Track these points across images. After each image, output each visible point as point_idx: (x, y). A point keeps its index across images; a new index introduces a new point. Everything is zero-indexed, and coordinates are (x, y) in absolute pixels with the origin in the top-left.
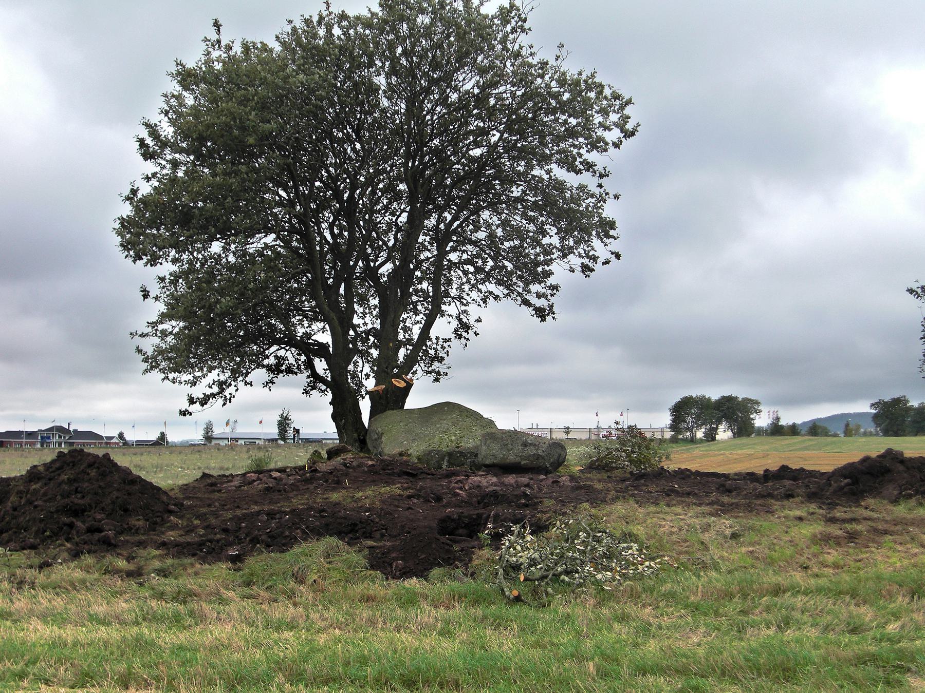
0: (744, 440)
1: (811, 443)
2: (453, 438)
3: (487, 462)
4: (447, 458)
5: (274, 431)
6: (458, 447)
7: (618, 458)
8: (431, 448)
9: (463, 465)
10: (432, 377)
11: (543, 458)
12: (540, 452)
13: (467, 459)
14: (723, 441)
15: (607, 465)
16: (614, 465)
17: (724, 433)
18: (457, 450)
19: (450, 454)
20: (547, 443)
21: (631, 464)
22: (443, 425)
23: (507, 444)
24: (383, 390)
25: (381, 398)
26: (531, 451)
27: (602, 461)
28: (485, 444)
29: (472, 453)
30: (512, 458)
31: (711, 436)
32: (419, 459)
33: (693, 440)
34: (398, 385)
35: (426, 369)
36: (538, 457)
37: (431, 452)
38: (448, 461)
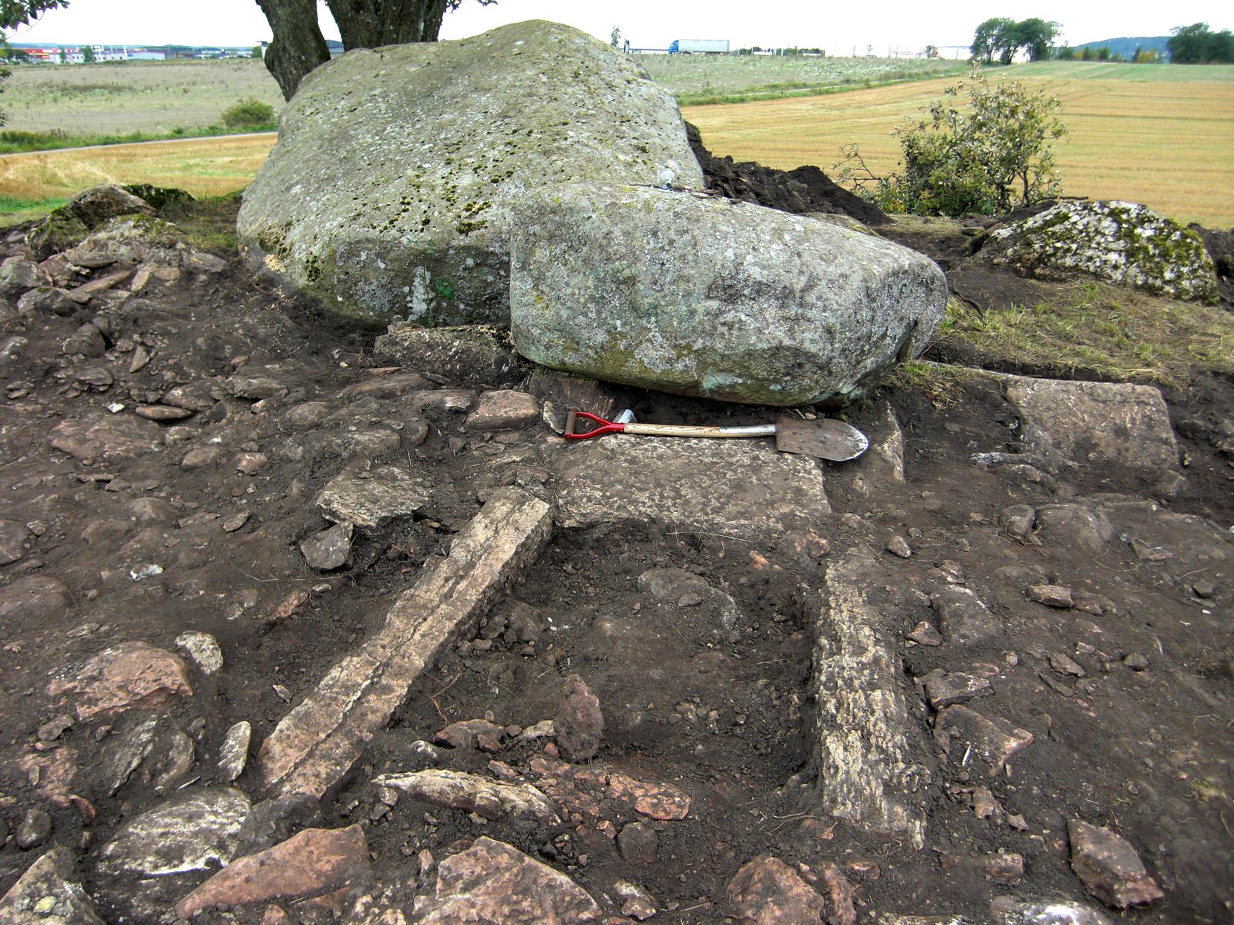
0: (1040, 65)
1: (1108, 70)
5: (609, 41)
6: (466, 229)
7: (1089, 235)
8: (359, 230)
11: (825, 367)
12: (810, 340)
14: (1022, 65)
15: (1042, 260)
16: (1069, 261)
17: (1021, 55)
18: (461, 240)
20: (856, 281)
21: (1129, 263)
23: (631, 281)
27: (1029, 244)
31: (1006, 60)
32: (314, 273)
33: (989, 63)
37: (353, 248)
38: (432, 286)
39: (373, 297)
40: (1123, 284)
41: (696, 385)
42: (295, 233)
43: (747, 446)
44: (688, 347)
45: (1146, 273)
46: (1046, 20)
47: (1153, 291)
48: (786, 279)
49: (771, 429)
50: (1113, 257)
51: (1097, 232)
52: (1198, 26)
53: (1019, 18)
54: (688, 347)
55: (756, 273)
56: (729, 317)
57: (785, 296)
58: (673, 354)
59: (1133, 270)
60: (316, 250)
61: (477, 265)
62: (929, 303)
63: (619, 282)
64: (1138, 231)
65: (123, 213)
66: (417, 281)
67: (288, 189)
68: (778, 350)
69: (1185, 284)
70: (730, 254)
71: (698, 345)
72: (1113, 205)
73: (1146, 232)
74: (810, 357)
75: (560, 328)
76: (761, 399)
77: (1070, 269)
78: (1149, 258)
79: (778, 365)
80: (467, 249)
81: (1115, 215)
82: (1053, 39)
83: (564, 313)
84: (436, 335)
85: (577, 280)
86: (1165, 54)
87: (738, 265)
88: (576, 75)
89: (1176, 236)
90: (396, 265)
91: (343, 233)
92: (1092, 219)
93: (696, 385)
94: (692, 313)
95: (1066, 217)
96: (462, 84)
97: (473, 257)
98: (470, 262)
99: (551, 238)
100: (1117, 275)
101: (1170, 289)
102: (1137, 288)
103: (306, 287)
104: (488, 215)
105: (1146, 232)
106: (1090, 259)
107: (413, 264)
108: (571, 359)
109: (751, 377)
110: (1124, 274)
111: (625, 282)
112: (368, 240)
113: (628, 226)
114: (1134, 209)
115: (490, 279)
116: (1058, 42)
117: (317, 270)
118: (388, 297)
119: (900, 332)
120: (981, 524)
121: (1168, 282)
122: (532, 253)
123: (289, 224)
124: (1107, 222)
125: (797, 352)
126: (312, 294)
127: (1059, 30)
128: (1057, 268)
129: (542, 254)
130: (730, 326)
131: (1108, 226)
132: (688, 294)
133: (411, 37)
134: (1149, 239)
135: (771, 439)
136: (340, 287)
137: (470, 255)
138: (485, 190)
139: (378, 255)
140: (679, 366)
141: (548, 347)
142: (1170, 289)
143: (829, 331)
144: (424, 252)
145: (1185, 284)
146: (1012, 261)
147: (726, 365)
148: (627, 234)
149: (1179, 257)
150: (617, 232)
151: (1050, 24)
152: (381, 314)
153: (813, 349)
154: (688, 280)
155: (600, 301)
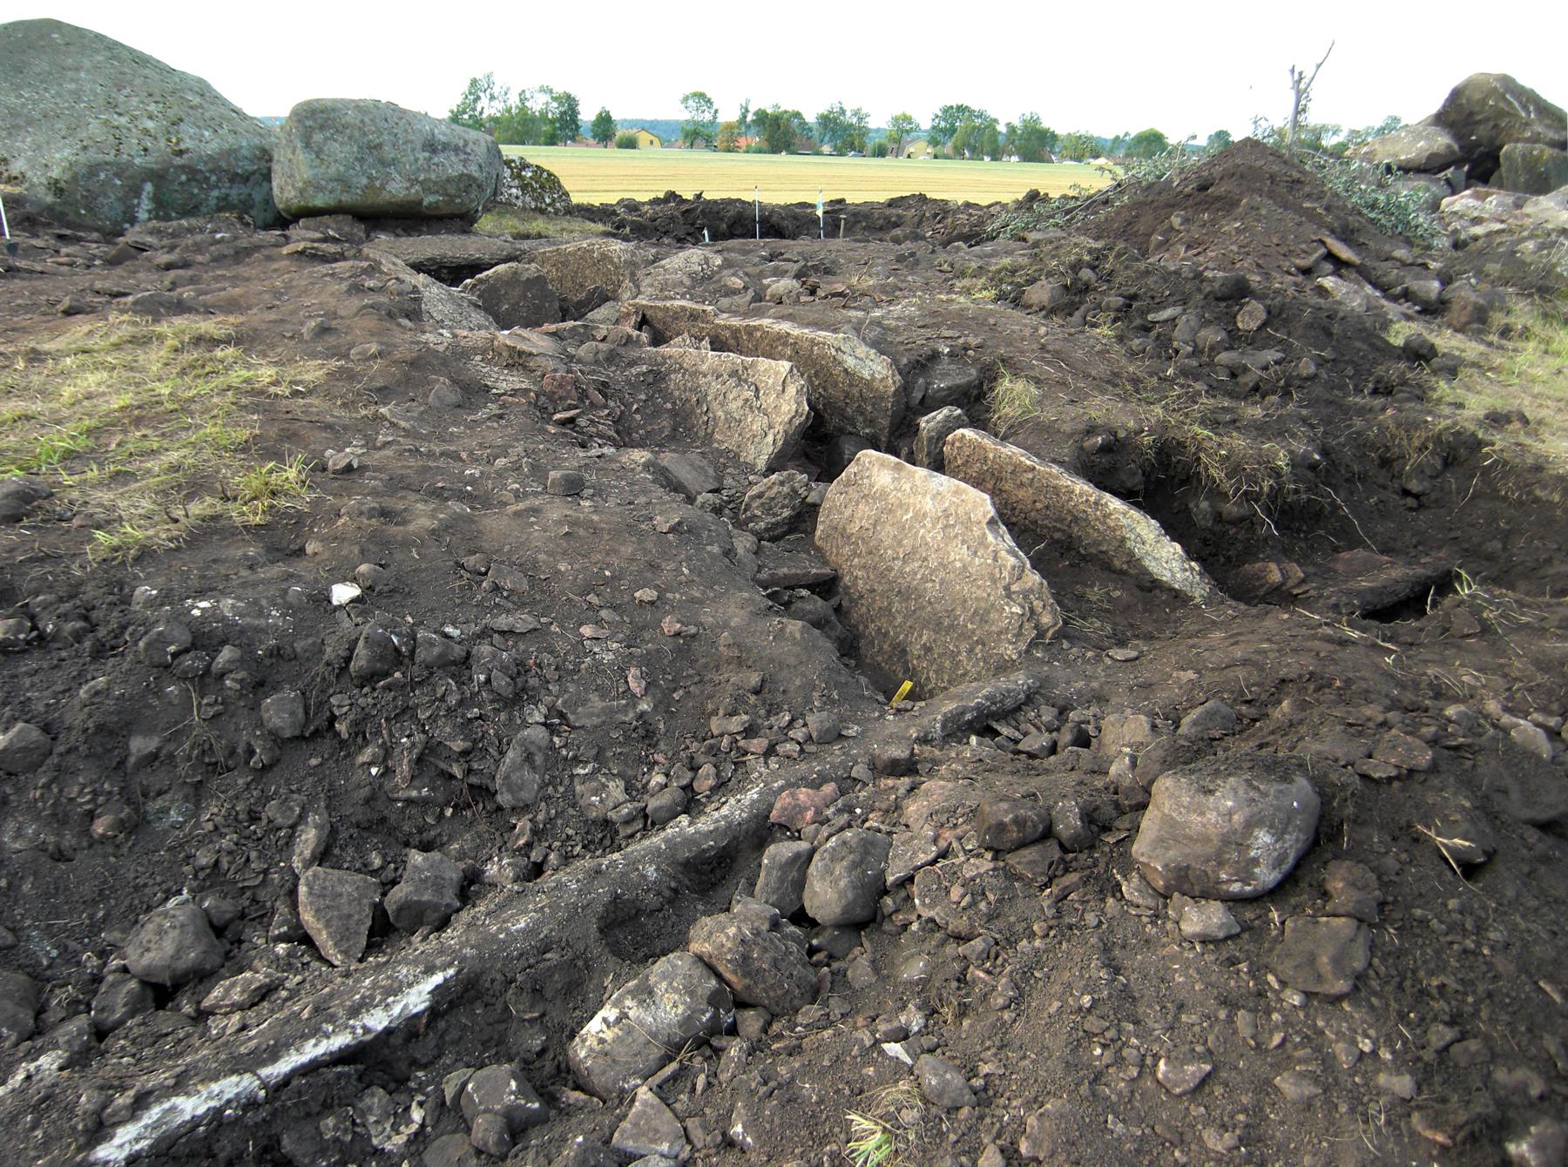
4: (149, 187)
8: (94, 156)
12: (473, 170)
18: (178, 161)
19: (158, 177)
23: (379, 146)
26: (452, 167)
30: (397, 189)
37: (93, 170)
39: (111, 208)
40: (524, 209)
41: (420, 203)
53: (1135, 129)
55: (443, 139)
56: (436, 160)
57: (457, 150)
59: (528, 199)
60: (55, 173)
63: (370, 148)
68: (462, 175)
71: (422, 177)
73: (528, 174)
74: (475, 179)
75: (339, 179)
76: (446, 210)
78: (534, 190)
80: (183, 167)
93: (420, 203)
94: (417, 160)
98: (184, 178)
99: (322, 128)
100: (519, 203)
103: (54, 203)
105: (528, 174)
107: (144, 181)
108: (346, 198)
115: (196, 191)
120: (321, 764)
125: (470, 177)
126: (58, 208)
129: (318, 137)
132: (413, 150)
150: (366, 120)
152: (116, 223)
155: (361, 160)
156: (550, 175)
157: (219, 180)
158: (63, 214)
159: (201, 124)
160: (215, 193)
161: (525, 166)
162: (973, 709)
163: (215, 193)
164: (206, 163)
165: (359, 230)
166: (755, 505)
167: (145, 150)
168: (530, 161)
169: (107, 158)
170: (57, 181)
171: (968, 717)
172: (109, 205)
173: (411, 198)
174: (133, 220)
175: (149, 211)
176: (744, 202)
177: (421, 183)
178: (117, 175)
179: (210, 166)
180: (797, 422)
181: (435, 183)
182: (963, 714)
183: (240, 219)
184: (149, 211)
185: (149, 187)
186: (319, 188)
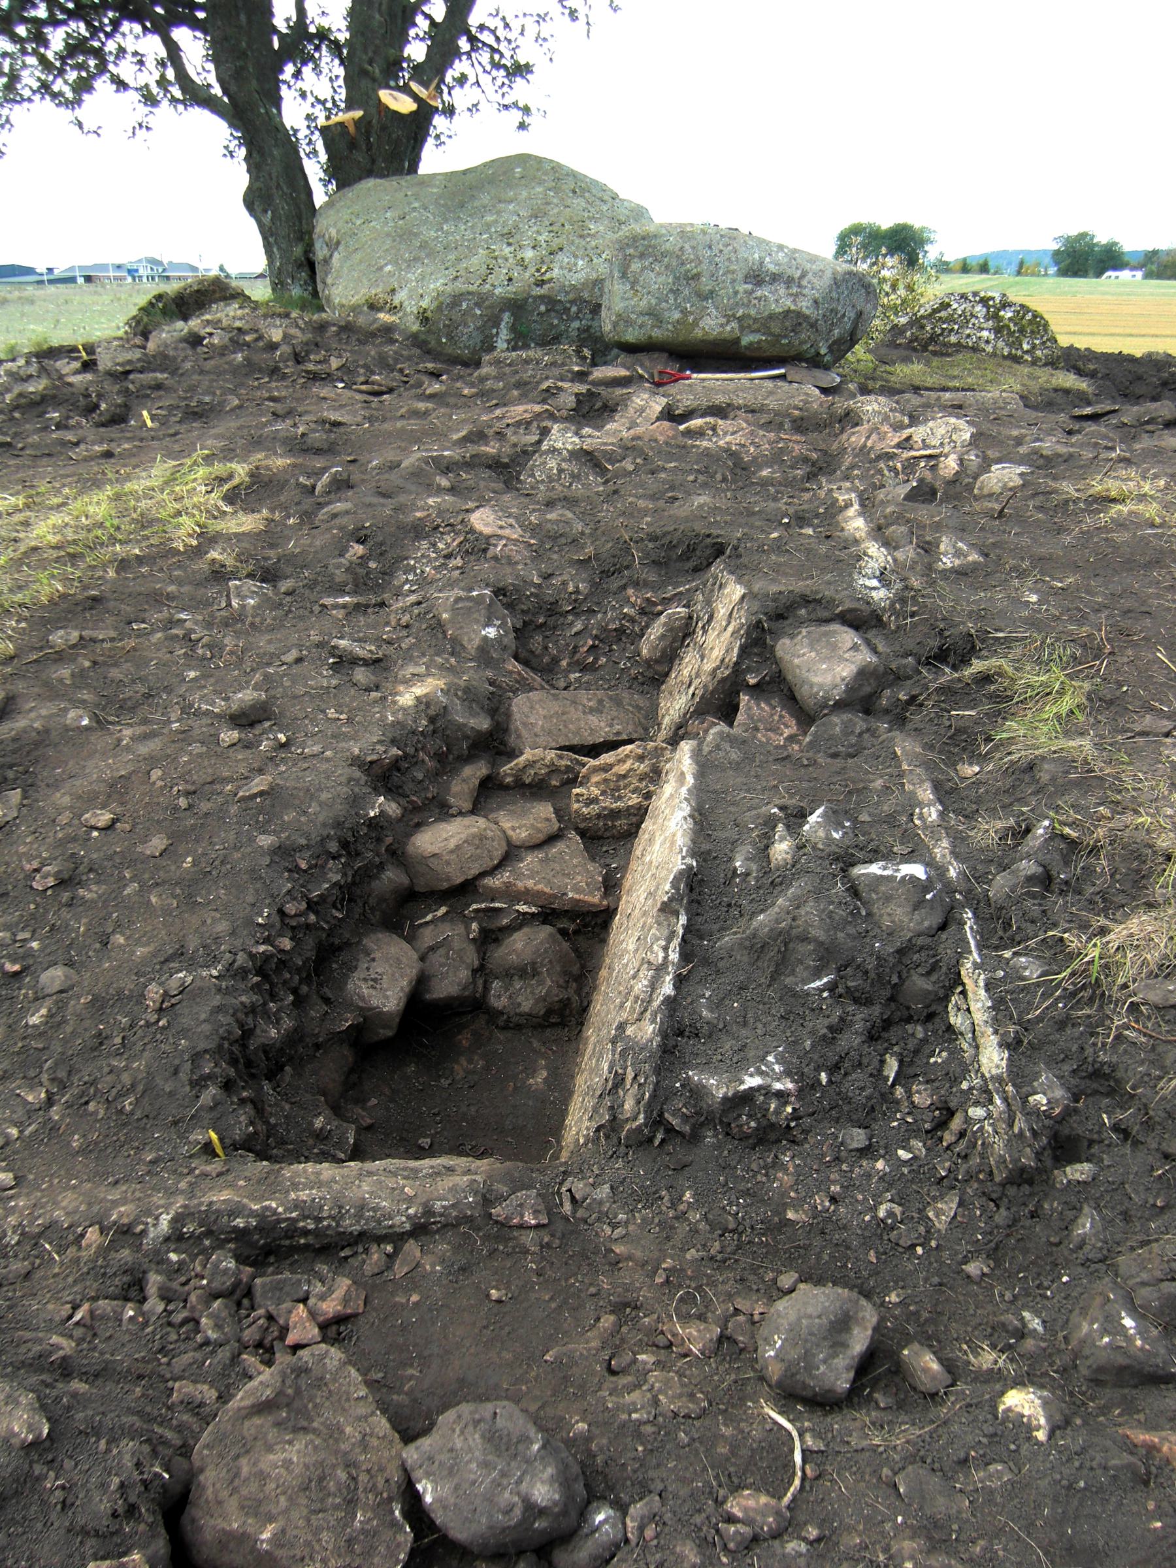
2: (529, 254)
3: (631, 336)
4: (506, 317)
6: (541, 283)
7: (966, 318)
8: (460, 286)
9: (556, 339)
10: (516, 116)
11: (813, 325)
12: (805, 305)
13: (571, 319)
15: (933, 338)
16: (953, 339)
18: (538, 291)
19: (517, 306)
22: (505, 216)
23: (697, 277)
24: (357, 123)
25: (353, 145)
26: (778, 300)
27: (923, 327)
28: (624, 275)
29: (579, 301)
34: (394, 106)
35: (498, 98)
36: (795, 319)
37: (457, 299)
38: (513, 329)
40: (994, 355)
41: (737, 341)
42: (401, 296)
43: (770, 384)
44: (734, 315)
45: (1010, 345)
46: (917, 225)
47: (1016, 360)
48: (789, 272)
49: (782, 371)
50: (985, 334)
51: (972, 315)
52: (1083, 236)
53: (886, 223)
54: (734, 315)
56: (759, 294)
57: (789, 281)
58: (724, 320)
59: (1001, 344)
60: (424, 304)
61: (548, 311)
62: (867, 301)
64: (1002, 313)
65: (224, 299)
66: (503, 324)
67: (381, 269)
68: (789, 311)
69: (1039, 353)
70: (756, 256)
72: (982, 294)
73: (1007, 314)
74: (806, 317)
75: (651, 313)
77: (954, 345)
78: (1011, 334)
79: (787, 324)
80: (542, 297)
81: (984, 301)
82: (927, 248)
83: (653, 301)
84: (531, 353)
85: (661, 279)
86: (1053, 270)
87: (762, 263)
88: (574, 192)
89: (1029, 316)
90: (489, 312)
91: (448, 289)
92: (967, 306)
93: (737, 341)
94: (736, 293)
95: (949, 305)
96: (485, 198)
97: (546, 304)
98: (543, 308)
99: (642, 256)
100: (989, 349)
101: (1028, 358)
102: (1004, 357)
104: (556, 273)
105: (1007, 314)
106: (969, 336)
107: (502, 311)
108: (657, 334)
109: (771, 334)
110: (995, 347)
111: (692, 278)
112: (469, 293)
113: (694, 243)
114: (997, 296)
115: (556, 322)
116: (931, 254)
117: (427, 319)
118: (481, 337)
119: (853, 315)
121: (1027, 352)
122: (629, 266)
123: (393, 291)
124: (979, 308)
125: (799, 314)
127: (932, 236)
128: (944, 345)
129: (636, 266)
130: (759, 299)
131: (980, 310)
132: (733, 281)
133: (399, 171)
134: (1010, 319)
135: (782, 377)
136: (445, 331)
137: (543, 303)
138: (547, 260)
139: (476, 304)
140: (728, 328)
141: (641, 327)
142: (1028, 358)
143: (816, 302)
144: (510, 300)
145: (1039, 353)
146: (911, 341)
147: (756, 326)
148: (693, 248)
149: (1032, 332)
150: (687, 246)
151: (923, 229)
153: (807, 312)
154: (733, 272)
156: (1036, 315)
157: (580, 311)
158: (425, 342)
159: (580, 253)
160: (576, 324)
161: (1005, 305)
162: (253, 1214)
163: (576, 324)
164: (567, 293)
165: (672, 368)
166: (595, 779)
167: (510, 280)
168: (1012, 298)
169: (471, 288)
170: (425, 310)
171: (240, 1222)
172: (468, 334)
173: (726, 336)
174: (492, 348)
175: (509, 342)
176: (1131, 359)
177: (740, 319)
178: (477, 304)
179: (571, 296)
180: (719, 675)
181: (755, 320)
182: (233, 1213)
183: (578, 352)
184: (509, 342)
185: (506, 317)
186: (629, 323)
